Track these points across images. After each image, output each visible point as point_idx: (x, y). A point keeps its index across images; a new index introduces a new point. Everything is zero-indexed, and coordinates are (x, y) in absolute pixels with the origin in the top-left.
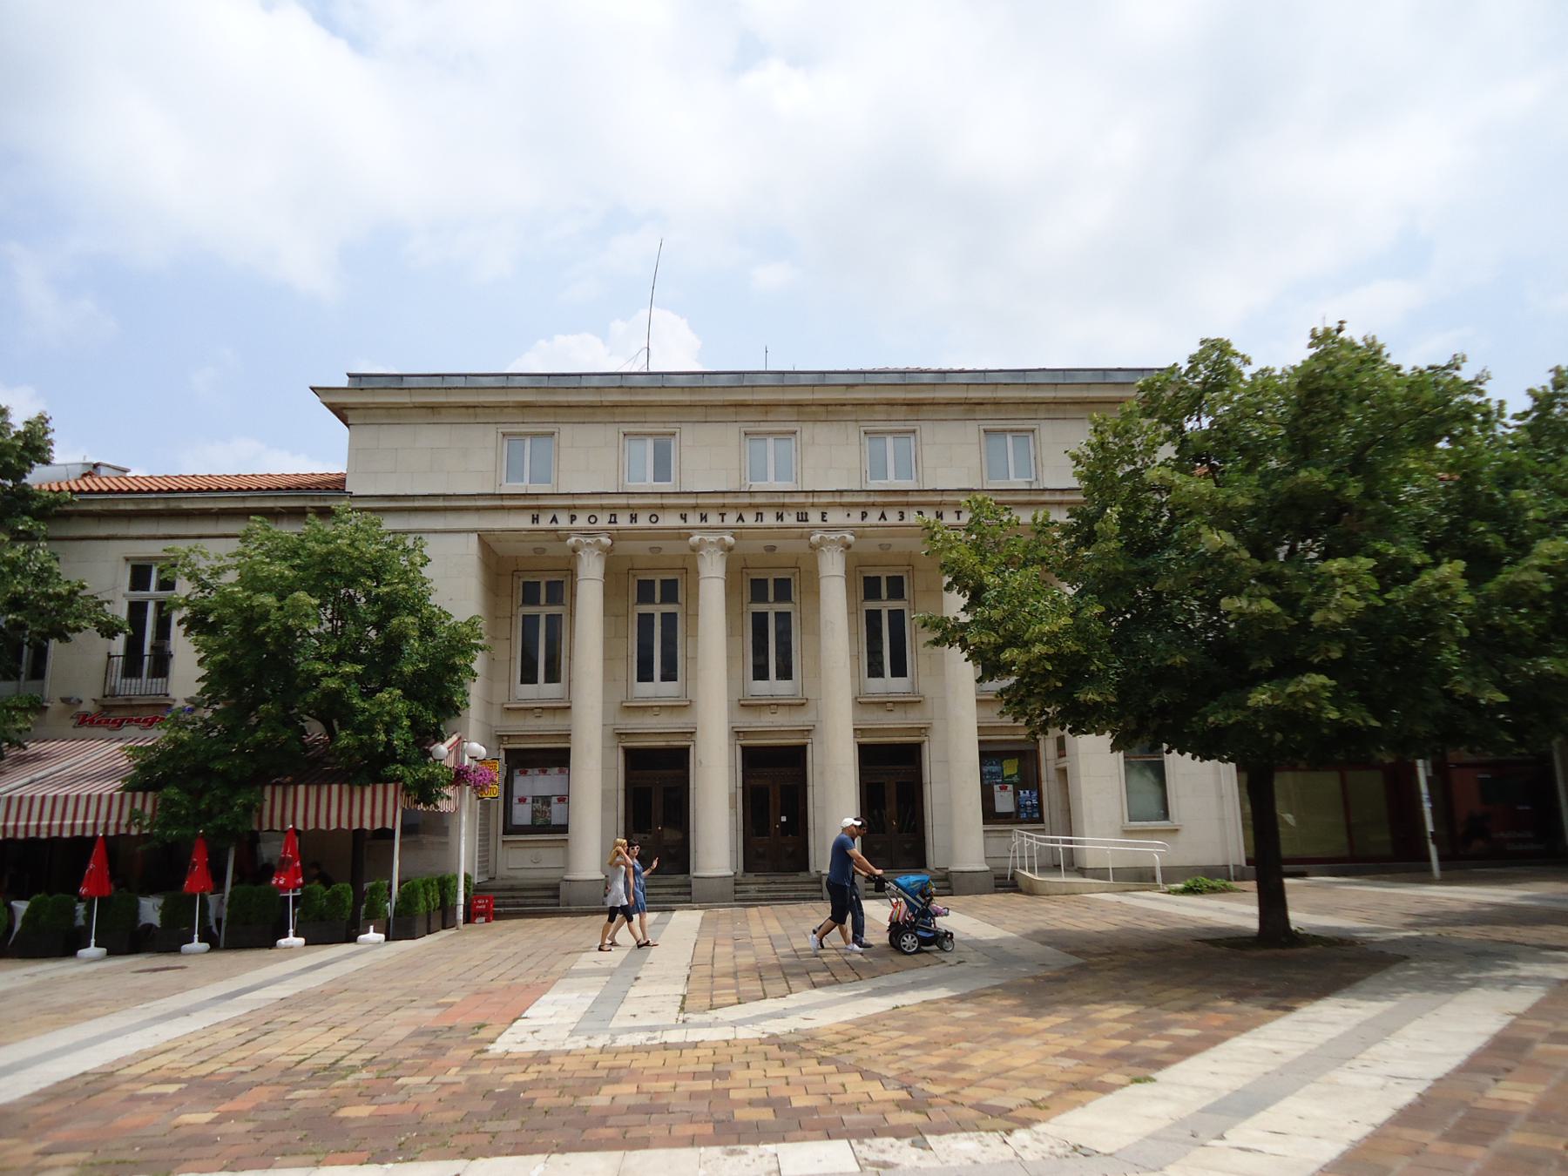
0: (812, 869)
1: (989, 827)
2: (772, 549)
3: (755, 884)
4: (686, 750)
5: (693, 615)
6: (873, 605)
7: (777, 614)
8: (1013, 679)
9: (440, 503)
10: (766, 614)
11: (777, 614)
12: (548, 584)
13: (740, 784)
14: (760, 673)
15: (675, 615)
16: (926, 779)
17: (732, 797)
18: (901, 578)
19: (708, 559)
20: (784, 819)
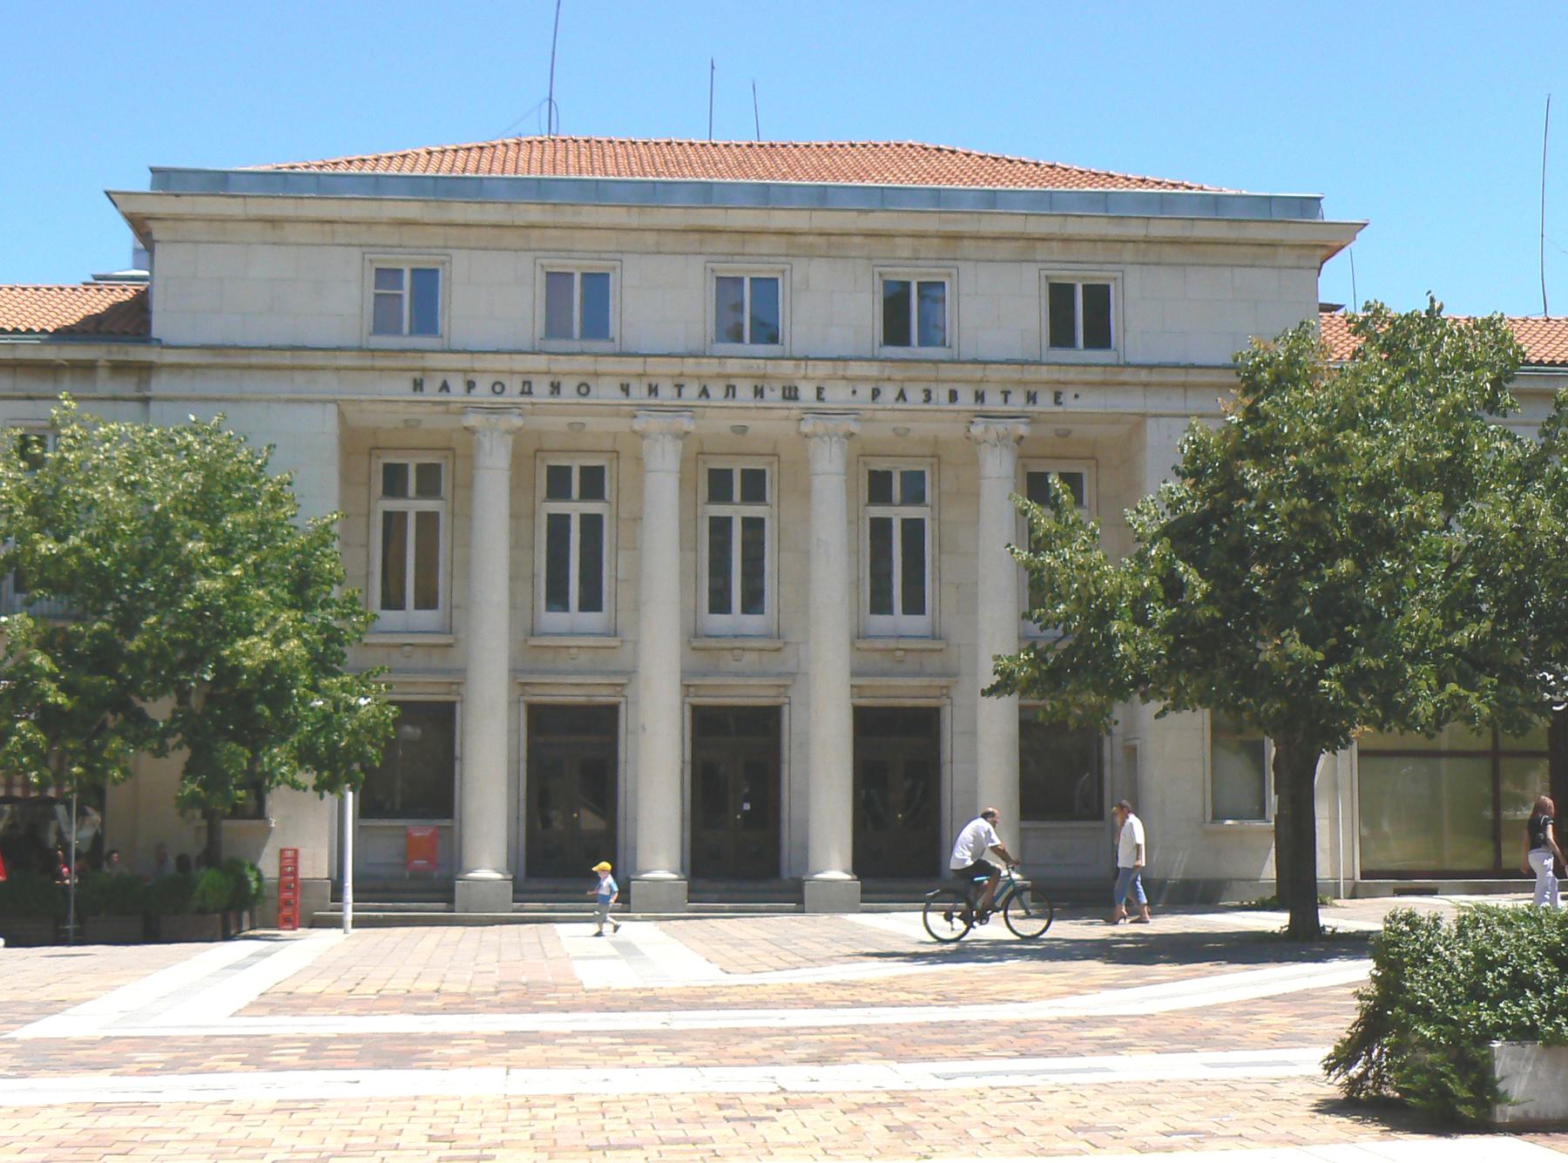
0: (785, 874)
1: (1027, 824)
2: (1067, 434)
3: (694, 894)
4: (613, 710)
5: (465, 514)
6: (879, 511)
7: (418, 514)
8: (1486, 625)
9: (286, 359)
10: (568, 516)
11: (418, 514)
12: (421, 468)
13: (458, 742)
14: (720, 603)
15: (921, 522)
16: (946, 755)
17: (512, 764)
18: (922, 474)
19: (487, 445)
20: (747, 806)
